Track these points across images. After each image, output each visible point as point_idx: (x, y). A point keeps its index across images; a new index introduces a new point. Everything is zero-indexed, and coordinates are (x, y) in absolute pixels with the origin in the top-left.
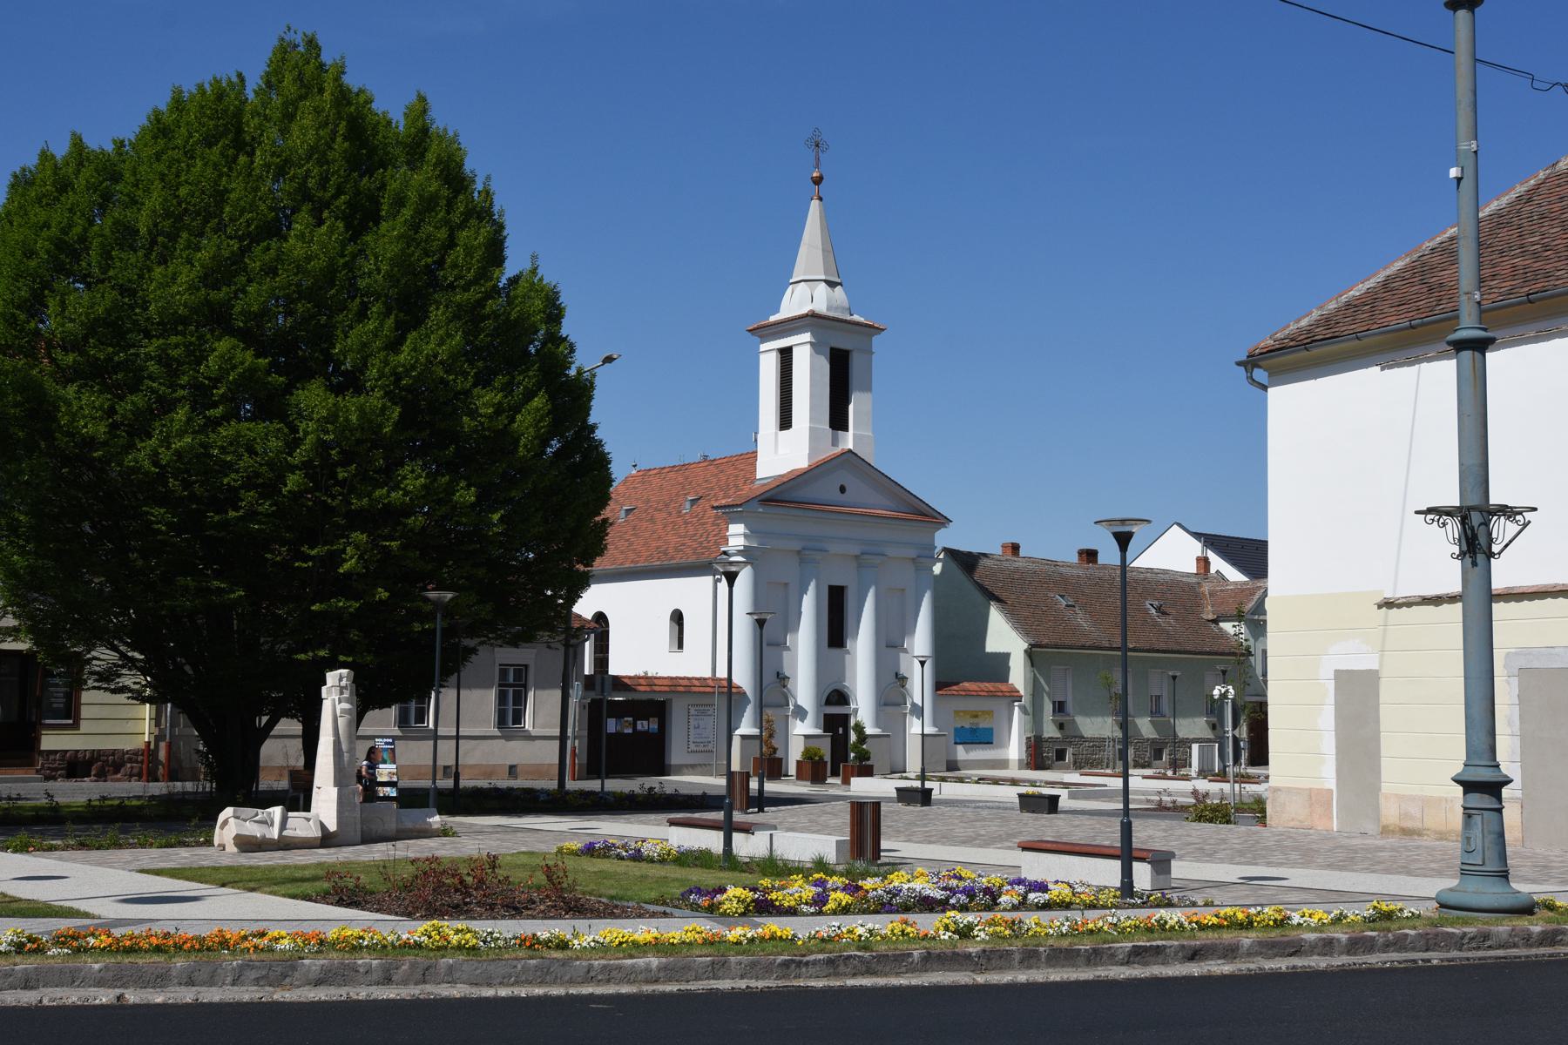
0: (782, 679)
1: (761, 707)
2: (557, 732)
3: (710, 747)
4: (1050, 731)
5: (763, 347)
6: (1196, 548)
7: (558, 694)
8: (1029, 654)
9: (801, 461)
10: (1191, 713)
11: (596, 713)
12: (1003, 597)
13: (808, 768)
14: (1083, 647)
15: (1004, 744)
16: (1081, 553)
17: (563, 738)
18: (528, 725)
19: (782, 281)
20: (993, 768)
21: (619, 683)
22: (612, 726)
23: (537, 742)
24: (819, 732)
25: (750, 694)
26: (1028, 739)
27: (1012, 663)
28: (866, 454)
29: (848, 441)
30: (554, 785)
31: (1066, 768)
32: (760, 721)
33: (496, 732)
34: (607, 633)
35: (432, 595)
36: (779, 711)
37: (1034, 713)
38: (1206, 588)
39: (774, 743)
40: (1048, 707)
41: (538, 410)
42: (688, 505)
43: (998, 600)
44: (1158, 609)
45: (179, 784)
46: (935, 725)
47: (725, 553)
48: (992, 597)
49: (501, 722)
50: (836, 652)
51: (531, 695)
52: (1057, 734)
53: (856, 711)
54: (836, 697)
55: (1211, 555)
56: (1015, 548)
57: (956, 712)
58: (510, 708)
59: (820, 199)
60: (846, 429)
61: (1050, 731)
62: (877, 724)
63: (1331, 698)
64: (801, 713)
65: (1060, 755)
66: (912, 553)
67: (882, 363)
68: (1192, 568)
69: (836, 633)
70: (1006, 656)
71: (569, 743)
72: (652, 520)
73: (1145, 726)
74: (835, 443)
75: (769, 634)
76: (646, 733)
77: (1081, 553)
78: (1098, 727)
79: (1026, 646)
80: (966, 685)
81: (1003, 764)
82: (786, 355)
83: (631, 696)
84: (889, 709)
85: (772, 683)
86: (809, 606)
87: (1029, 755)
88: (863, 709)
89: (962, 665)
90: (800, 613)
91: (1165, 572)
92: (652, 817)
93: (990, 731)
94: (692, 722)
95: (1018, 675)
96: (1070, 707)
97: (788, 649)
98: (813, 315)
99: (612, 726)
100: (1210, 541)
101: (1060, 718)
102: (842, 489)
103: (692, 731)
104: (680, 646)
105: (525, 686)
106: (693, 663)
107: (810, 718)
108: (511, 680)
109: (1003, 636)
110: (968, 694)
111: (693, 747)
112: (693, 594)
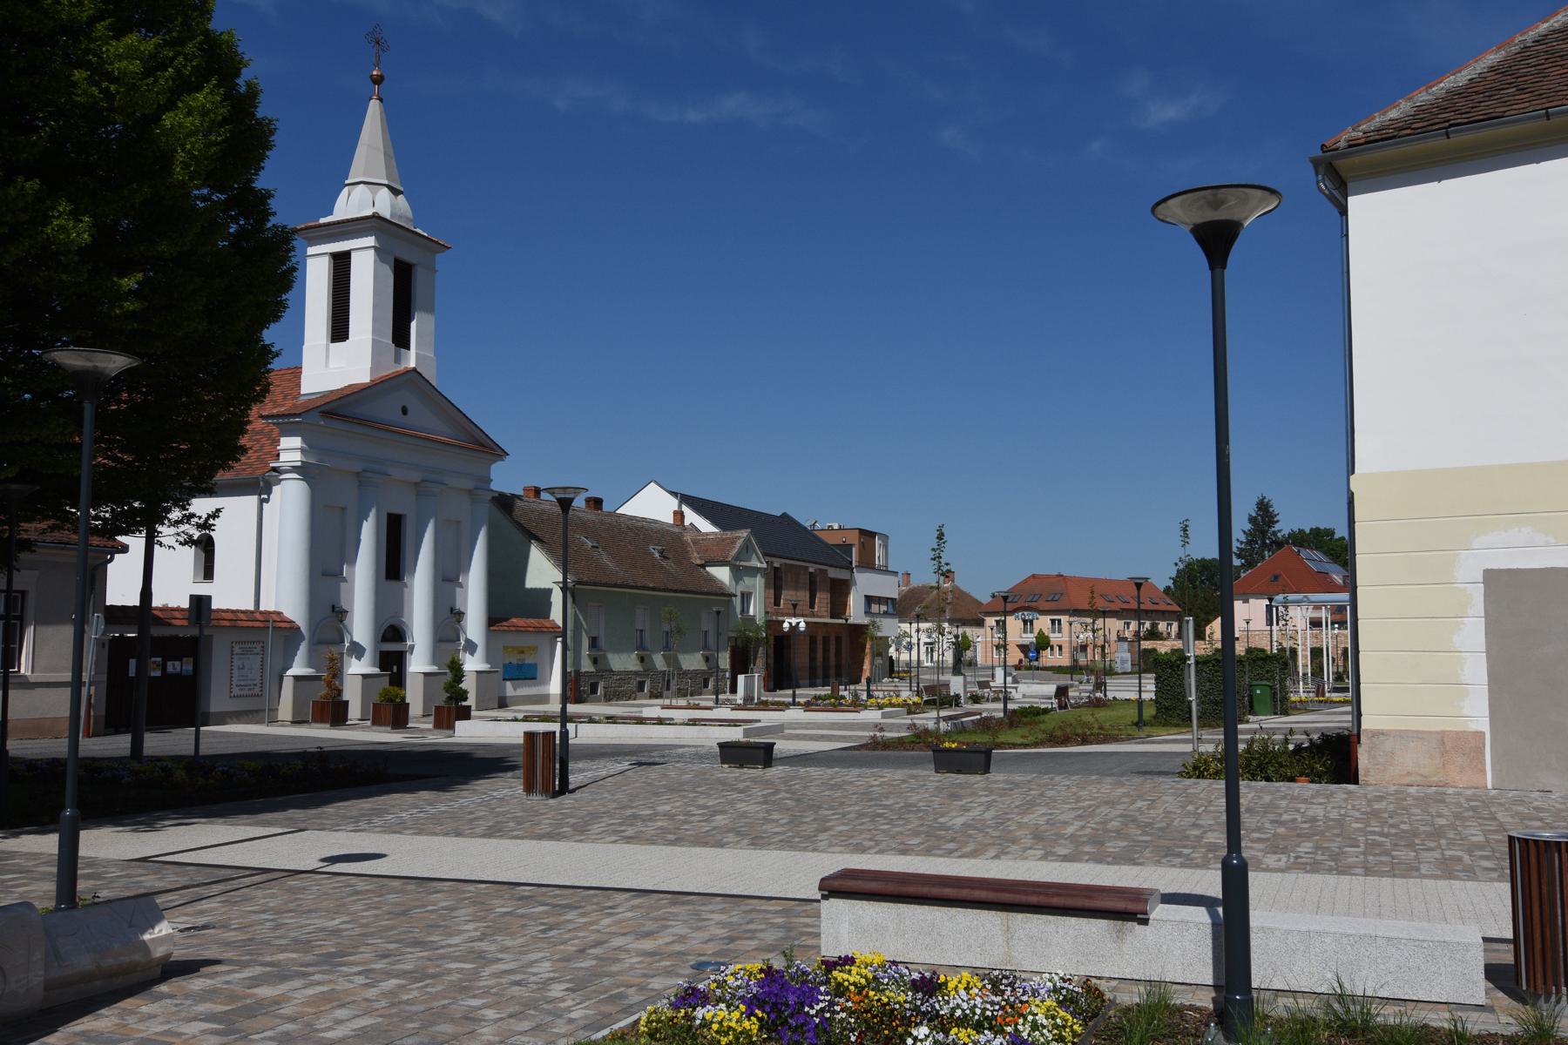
1: (317, 642)
2: (67, 676)
3: (257, 690)
4: (587, 666)
5: (311, 250)
6: (673, 503)
7: (68, 631)
9: (362, 376)
10: (690, 650)
11: (117, 652)
12: (540, 534)
14: (616, 586)
17: (76, 684)
19: (337, 180)
23: (39, 691)
24: (376, 670)
25: (304, 629)
28: (430, 374)
29: (411, 360)
31: (598, 701)
35: (72, 359)
38: (688, 538)
40: (585, 643)
41: (204, 113)
43: (538, 540)
44: (661, 553)
46: (488, 661)
47: (274, 469)
50: (393, 584)
51: (29, 632)
52: (592, 669)
55: (685, 509)
59: (381, 100)
60: (408, 348)
61: (587, 666)
63: (1479, 607)
64: (357, 651)
65: (594, 690)
67: (441, 280)
68: (669, 519)
69: (393, 567)
71: (84, 691)
73: (659, 661)
74: (398, 360)
76: (179, 675)
78: (624, 662)
81: (544, 699)
82: (341, 263)
84: (444, 646)
85: (328, 613)
86: (368, 534)
89: (511, 603)
90: (358, 541)
91: (656, 522)
92: (329, 809)
93: (534, 666)
94: (237, 663)
96: (602, 642)
97: (345, 580)
98: (376, 216)
100: (685, 499)
101: (595, 653)
102: (405, 411)
103: (236, 671)
105: (21, 618)
107: (480, 651)
109: (542, 572)
110: (519, 630)
111: (236, 691)
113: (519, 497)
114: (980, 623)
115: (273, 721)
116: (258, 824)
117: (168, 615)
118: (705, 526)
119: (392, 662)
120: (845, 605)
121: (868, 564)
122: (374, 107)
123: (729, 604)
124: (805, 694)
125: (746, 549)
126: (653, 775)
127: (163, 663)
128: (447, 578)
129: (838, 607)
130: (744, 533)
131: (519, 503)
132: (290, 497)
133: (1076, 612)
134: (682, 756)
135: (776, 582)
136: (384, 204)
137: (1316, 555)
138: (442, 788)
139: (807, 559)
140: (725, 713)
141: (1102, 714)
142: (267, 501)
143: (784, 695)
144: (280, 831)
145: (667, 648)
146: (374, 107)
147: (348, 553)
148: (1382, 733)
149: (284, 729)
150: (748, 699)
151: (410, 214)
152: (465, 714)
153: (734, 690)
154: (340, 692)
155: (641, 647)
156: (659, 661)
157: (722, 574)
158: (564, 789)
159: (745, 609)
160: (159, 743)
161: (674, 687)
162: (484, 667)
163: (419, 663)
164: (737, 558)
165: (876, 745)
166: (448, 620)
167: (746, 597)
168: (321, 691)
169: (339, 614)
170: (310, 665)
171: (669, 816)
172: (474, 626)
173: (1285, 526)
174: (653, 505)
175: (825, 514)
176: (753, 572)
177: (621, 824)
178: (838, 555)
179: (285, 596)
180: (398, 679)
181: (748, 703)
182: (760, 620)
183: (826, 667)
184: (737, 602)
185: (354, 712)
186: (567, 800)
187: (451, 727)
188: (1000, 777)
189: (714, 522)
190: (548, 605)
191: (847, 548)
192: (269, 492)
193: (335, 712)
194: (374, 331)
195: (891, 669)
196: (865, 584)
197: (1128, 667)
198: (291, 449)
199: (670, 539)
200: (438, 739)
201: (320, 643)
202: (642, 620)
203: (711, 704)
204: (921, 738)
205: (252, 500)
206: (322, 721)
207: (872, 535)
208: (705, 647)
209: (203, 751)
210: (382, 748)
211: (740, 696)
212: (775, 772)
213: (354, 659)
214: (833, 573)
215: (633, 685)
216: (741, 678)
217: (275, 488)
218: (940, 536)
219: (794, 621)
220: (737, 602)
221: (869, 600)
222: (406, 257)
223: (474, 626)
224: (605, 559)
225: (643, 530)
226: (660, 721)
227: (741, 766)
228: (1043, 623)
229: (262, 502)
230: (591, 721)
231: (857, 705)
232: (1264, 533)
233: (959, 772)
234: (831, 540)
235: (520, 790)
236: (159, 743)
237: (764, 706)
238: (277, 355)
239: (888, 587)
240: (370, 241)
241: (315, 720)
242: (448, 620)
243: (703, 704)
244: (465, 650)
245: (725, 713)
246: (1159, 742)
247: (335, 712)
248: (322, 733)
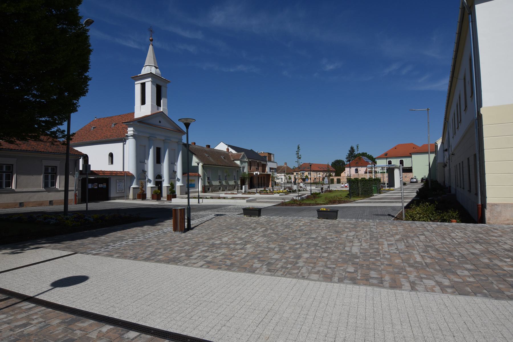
1: (139, 179)
3: (123, 191)
4: (207, 184)
5: (136, 83)
6: (227, 147)
9: (149, 113)
13: (156, 196)
16: (207, 146)
18: (57, 186)
19: (142, 66)
20: (480, 177)
21: (93, 173)
22: (90, 186)
24: (155, 186)
25: (135, 176)
28: (166, 113)
29: (161, 109)
30: (61, 208)
31: (210, 192)
33: (44, 189)
37: (204, 180)
38: (230, 154)
39: (144, 189)
40: (206, 179)
42: (113, 125)
43: (195, 154)
45: (362, 170)
49: (46, 186)
51: (58, 177)
56: (195, 143)
58: (50, 181)
64: (150, 181)
65: (209, 189)
69: (158, 160)
72: (102, 129)
73: (224, 183)
74: (158, 109)
76: (102, 188)
77: (207, 146)
78: (216, 183)
82: (143, 85)
83: (97, 177)
93: (194, 184)
96: (210, 178)
98: (151, 73)
100: (229, 146)
102: (160, 122)
104: (112, 163)
105: (56, 173)
106: (117, 167)
107: (152, 182)
108: (50, 171)
111: (118, 191)
112: (116, 148)
114: (293, 174)
115: (127, 198)
116: (63, 249)
118: (234, 152)
119: (159, 184)
120: (265, 170)
121: (270, 160)
123: (240, 169)
124: (259, 189)
125: (243, 156)
126: (221, 220)
127: (97, 185)
129: (264, 170)
130: (243, 153)
132: (131, 143)
133: (314, 171)
134: (230, 209)
135: (250, 164)
136: (153, 70)
137: (365, 158)
138: (153, 224)
139: (257, 160)
140: (240, 195)
141: (332, 195)
143: (254, 190)
144: (70, 253)
145: (226, 179)
147: (146, 157)
148: (496, 205)
149: (131, 201)
150: (245, 191)
151: (160, 73)
152: (175, 197)
153: (242, 189)
155: (220, 179)
156: (224, 183)
157: (238, 162)
158: (189, 228)
159: (243, 170)
160: (93, 206)
161: (227, 188)
162: (182, 185)
163: (165, 184)
164: (241, 159)
165: (283, 204)
166: (172, 174)
167: (244, 168)
168: (139, 191)
169: (144, 172)
170: (137, 184)
171: (227, 244)
173: (356, 152)
174: (222, 147)
175: (260, 149)
176: (245, 162)
177: (206, 251)
178: (263, 158)
179: (130, 168)
180: (160, 188)
181: (245, 193)
182: (247, 173)
183: (261, 184)
184: (242, 169)
185: (149, 195)
186: (189, 234)
187: (171, 200)
188: (343, 221)
189: (236, 151)
191: (265, 157)
193: (143, 196)
195: (276, 184)
196: (269, 165)
197: (327, 183)
198: (130, 131)
199: (226, 155)
200: (167, 203)
201: (140, 179)
202: (220, 173)
203: (236, 193)
204: (293, 202)
205: (122, 144)
206: (140, 199)
207: (271, 154)
208: (235, 179)
209: (88, 209)
210: (149, 207)
211: (243, 190)
212: (263, 218)
214: (263, 162)
215: (218, 188)
216: (243, 186)
217: (127, 141)
218: (298, 148)
219: (256, 172)
220: (242, 169)
221: (271, 169)
222: (160, 84)
223: (179, 175)
224: (211, 159)
225: (220, 153)
226: (224, 198)
227: (251, 216)
228: (306, 173)
229: (124, 144)
230: (207, 198)
231: (272, 193)
232: (352, 154)
233: (327, 219)
234: (262, 155)
235: (171, 228)
236: (93, 206)
237: (250, 193)
238: (90, 80)
239: (274, 166)
240: (150, 79)
241: (138, 198)
242: (172, 174)
243: (235, 193)
245: (240, 195)
246: (357, 203)
247: (143, 196)
248: (140, 202)
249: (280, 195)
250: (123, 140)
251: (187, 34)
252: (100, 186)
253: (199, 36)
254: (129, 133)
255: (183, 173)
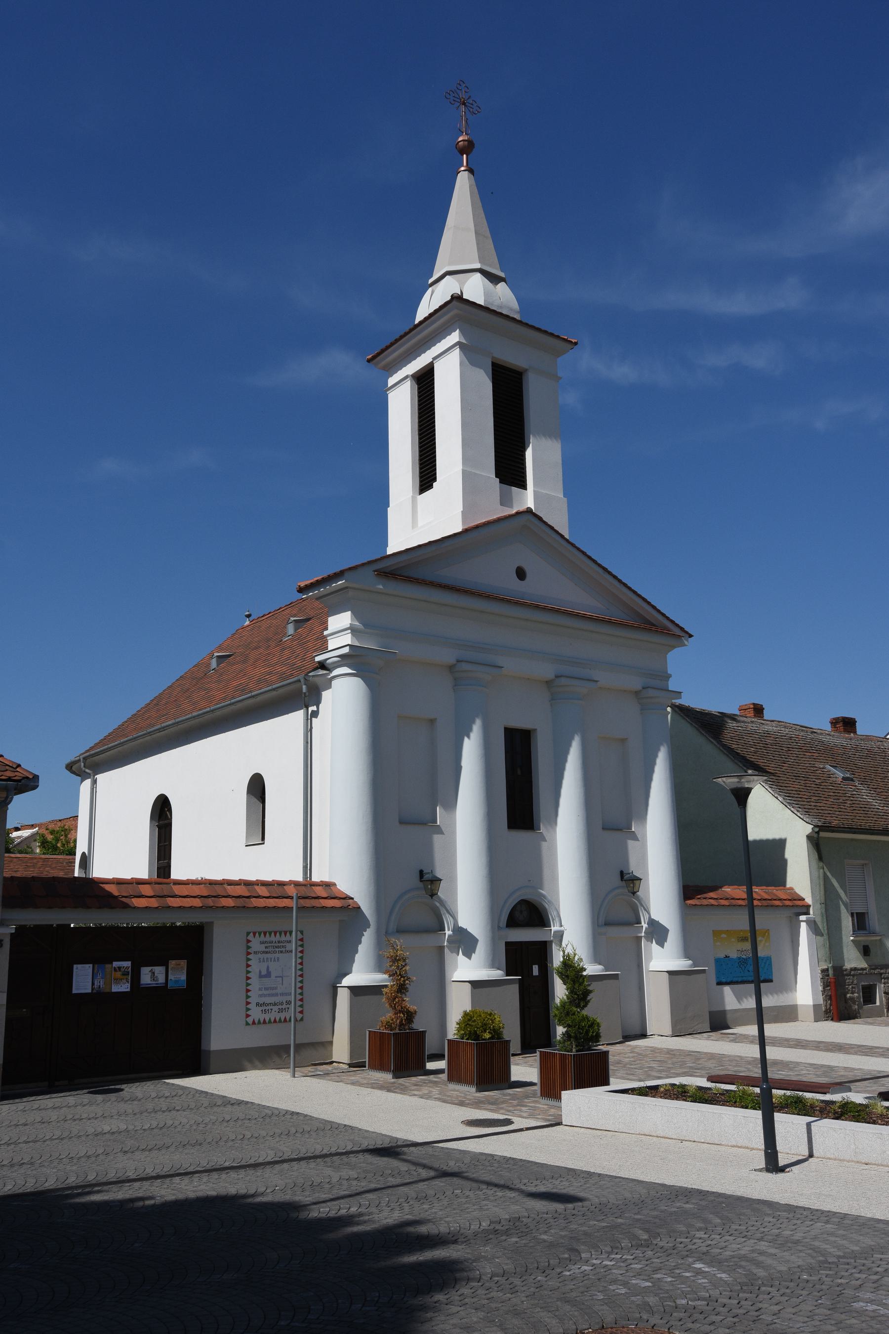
0: (429, 883)
4: (853, 960)
5: (391, 381)
8: (814, 841)
12: (761, 762)
15: (789, 986)
16: (835, 722)
24: (497, 974)
26: (825, 971)
27: (789, 854)
28: (559, 519)
29: (528, 499)
32: (393, 962)
34: (170, 825)
36: (429, 940)
37: (826, 931)
39: (410, 1002)
40: (847, 923)
42: (291, 629)
43: (761, 770)
46: (687, 955)
48: (748, 764)
52: (863, 965)
53: (560, 935)
54: (523, 914)
56: (758, 710)
57: (716, 933)
60: (523, 486)
61: (853, 960)
62: (597, 958)
64: (465, 942)
65: (869, 996)
66: (635, 683)
69: (520, 806)
70: (780, 844)
74: (505, 500)
75: (402, 811)
76: (161, 992)
77: (835, 722)
79: (809, 829)
80: (727, 889)
84: (613, 931)
87: (828, 997)
88: (572, 930)
94: (256, 966)
95: (800, 875)
96: (874, 921)
99: (83, 979)
102: (521, 574)
103: (255, 983)
106: (275, 862)
107: (674, 938)
109: (769, 816)
111: (256, 1014)
112: (268, 744)
113: (733, 717)
117: (129, 890)
122: (463, 182)
128: (611, 827)
131: (731, 724)
132: (344, 700)
142: (315, 714)
146: (463, 182)
151: (515, 305)
154: (410, 1016)
168: (384, 1015)
172: (660, 896)
179: (343, 863)
190: (782, 864)
192: (318, 703)
194: (466, 459)
205: (298, 716)
213: (461, 958)
217: (326, 695)
222: (513, 357)
224: (865, 795)
244: (650, 936)
249: (266, 947)
250: (300, 694)
251: (739, 304)
252: (147, 976)
253: (791, 297)
254: (332, 644)
255: (691, 890)
